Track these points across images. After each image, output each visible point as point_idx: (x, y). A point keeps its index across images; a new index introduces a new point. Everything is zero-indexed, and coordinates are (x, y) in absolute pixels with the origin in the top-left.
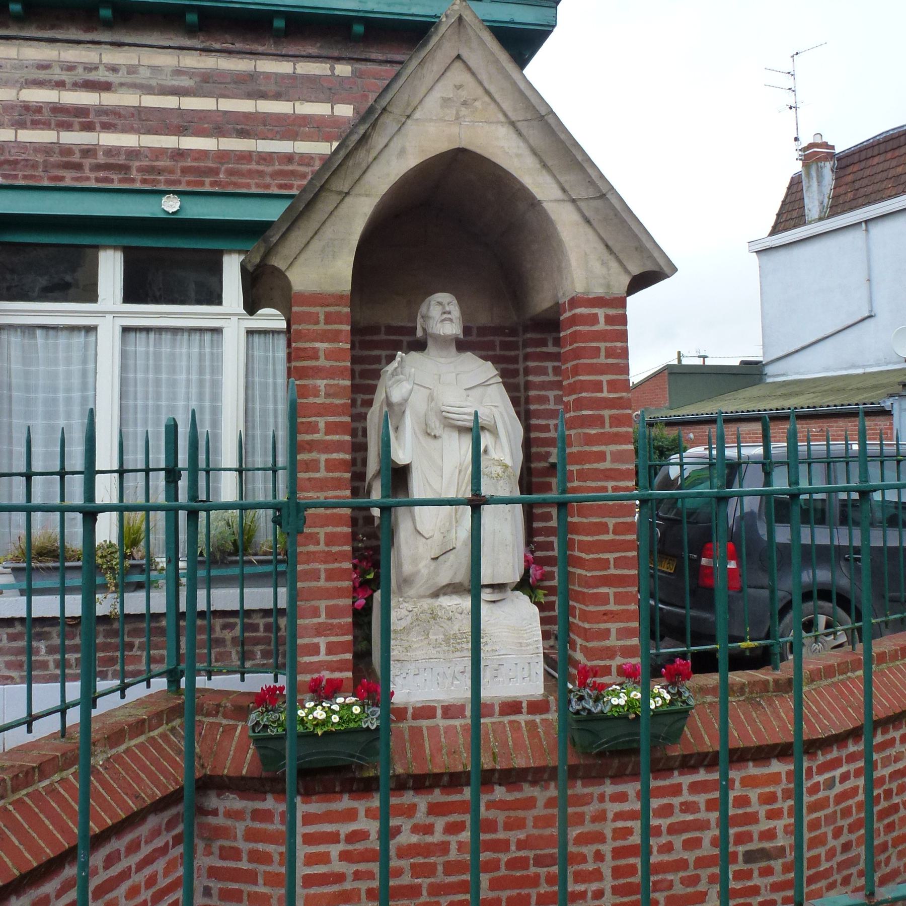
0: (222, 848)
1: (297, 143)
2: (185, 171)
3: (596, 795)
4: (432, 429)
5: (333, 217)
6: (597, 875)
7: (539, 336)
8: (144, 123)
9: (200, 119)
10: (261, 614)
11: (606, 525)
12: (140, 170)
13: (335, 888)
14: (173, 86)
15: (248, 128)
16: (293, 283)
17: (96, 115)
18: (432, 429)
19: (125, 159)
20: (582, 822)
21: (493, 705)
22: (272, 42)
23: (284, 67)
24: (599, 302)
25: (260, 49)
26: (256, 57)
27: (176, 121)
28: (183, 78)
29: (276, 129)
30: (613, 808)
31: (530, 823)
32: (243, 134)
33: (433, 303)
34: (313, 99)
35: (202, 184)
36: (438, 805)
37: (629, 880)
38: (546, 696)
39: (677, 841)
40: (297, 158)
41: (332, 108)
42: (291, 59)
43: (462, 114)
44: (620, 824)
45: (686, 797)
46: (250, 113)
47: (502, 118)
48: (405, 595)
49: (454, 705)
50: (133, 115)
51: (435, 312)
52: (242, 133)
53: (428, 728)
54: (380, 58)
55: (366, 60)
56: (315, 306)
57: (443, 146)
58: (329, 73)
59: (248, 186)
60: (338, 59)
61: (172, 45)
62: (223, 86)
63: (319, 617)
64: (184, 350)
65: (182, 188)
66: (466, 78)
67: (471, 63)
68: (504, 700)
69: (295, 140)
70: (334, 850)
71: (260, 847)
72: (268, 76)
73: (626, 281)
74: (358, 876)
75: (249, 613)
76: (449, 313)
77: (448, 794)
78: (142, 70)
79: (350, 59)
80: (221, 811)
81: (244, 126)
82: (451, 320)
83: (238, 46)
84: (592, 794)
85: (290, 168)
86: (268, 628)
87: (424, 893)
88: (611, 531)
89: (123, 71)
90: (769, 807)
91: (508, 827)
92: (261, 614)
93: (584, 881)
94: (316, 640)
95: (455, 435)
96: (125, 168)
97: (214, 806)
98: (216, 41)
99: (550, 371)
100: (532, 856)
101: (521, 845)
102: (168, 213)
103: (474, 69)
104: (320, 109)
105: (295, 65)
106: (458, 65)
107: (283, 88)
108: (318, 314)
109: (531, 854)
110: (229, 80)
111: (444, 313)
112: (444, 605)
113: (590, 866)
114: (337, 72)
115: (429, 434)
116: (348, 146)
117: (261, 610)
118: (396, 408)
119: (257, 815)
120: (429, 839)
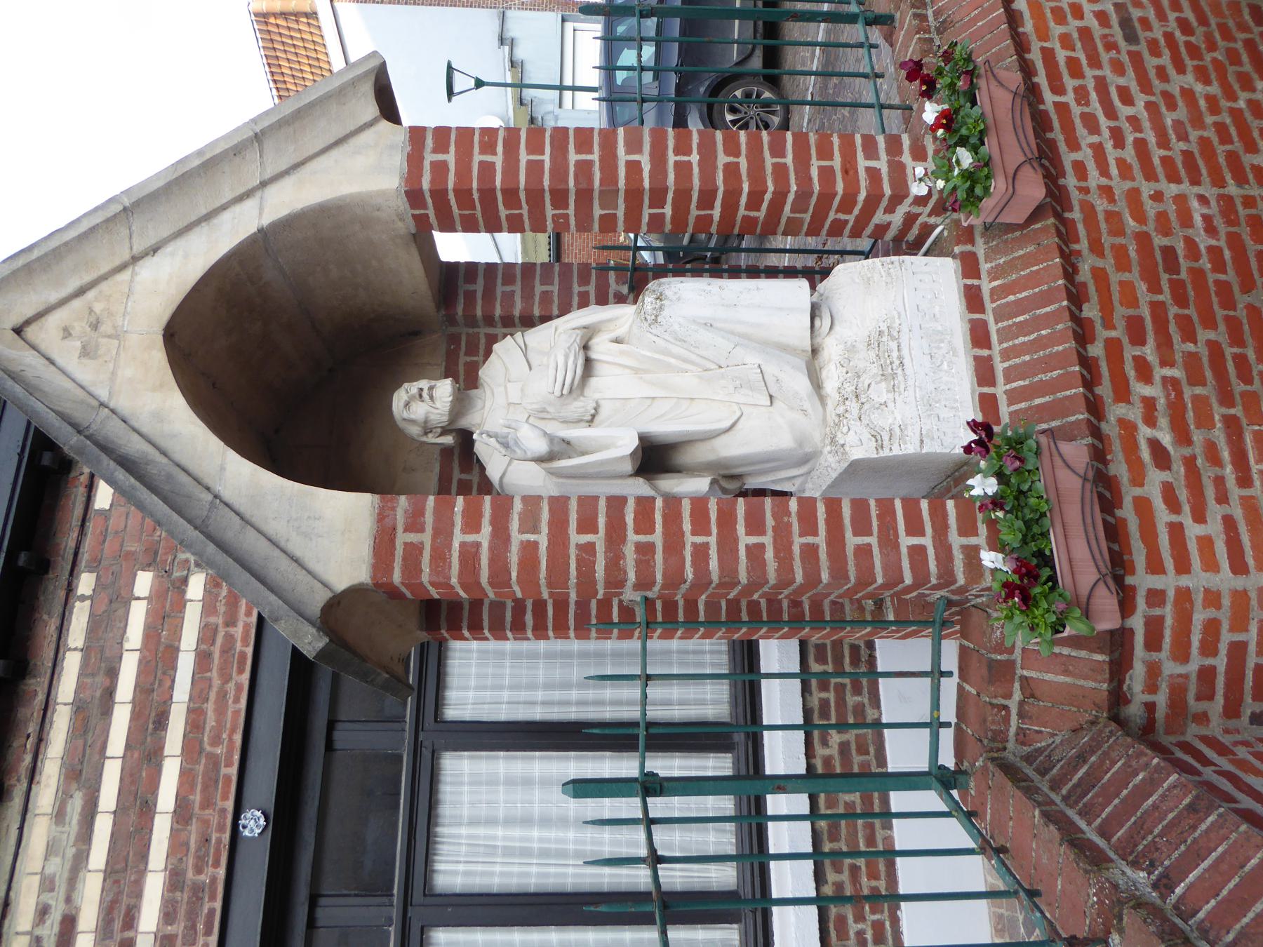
0: (1199, 698)
1: (183, 646)
2: (207, 803)
3: (1081, 196)
4: (586, 411)
5: (254, 520)
6: (1181, 199)
7: (461, 301)
8: (130, 864)
9: (133, 782)
10: (807, 695)
11: (727, 166)
12: (199, 870)
13: (1243, 529)
14: (80, 823)
15: (153, 714)
16: (355, 581)
17: (111, 938)
18: (586, 411)
19: (182, 892)
20: (1118, 215)
21: (971, 321)
22: (32, 681)
23: (72, 663)
24: (414, 160)
25: (41, 697)
26: (51, 703)
27: (133, 817)
28: (69, 809)
29: (159, 674)
30: (1094, 179)
31: (1126, 276)
32: (161, 721)
33: (405, 415)
34: (122, 625)
35: (228, 778)
36: (1115, 391)
37: (1180, 166)
38: (954, 257)
39: (1124, 111)
40: (204, 647)
41: (138, 598)
42: (60, 655)
43: (110, 331)
44: (1114, 171)
45: (1069, 98)
46: (133, 712)
47: (125, 276)
48: (820, 445)
49: (977, 370)
50: (117, 882)
51: (419, 411)
52: (160, 723)
53: (1010, 404)
54: (75, 535)
55: (76, 554)
56: (394, 547)
57: (158, 357)
58: (88, 603)
59: (236, 712)
60: (70, 589)
61: (17, 825)
62: (88, 752)
63: (869, 545)
64: (464, 831)
65: (230, 805)
66: (54, 321)
67: (30, 313)
68: (964, 307)
69: (178, 650)
70: (1193, 531)
71: (1196, 639)
72: (80, 687)
73: (385, 125)
74: (1222, 498)
75: (807, 712)
76: (421, 390)
77: (1100, 376)
78: (50, 869)
79: (71, 574)
80: (1148, 698)
81: (150, 718)
82: (431, 388)
83: (32, 728)
84: (1081, 201)
85: (216, 655)
86: (824, 687)
87: (1232, 411)
88: (736, 160)
89: (48, 898)
90: (1069, 16)
91: (1134, 303)
92: (807, 695)
93: (1191, 218)
94: (904, 550)
95: (593, 382)
96: (197, 890)
97: (1143, 708)
98: (20, 760)
99: (508, 288)
100: (1167, 276)
101: (1155, 288)
102: (266, 827)
103: (41, 308)
104: (138, 615)
105: (69, 649)
106: (30, 332)
107: (102, 666)
108: (405, 544)
109: (1164, 277)
110: (80, 742)
111: (421, 396)
112: (837, 384)
113: (1172, 208)
114: (89, 592)
115: (593, 416)
116: (133, 488)
117: (803, 696)
118: (556, 448)
119: (1153, 642)
120: (1161, 403)
